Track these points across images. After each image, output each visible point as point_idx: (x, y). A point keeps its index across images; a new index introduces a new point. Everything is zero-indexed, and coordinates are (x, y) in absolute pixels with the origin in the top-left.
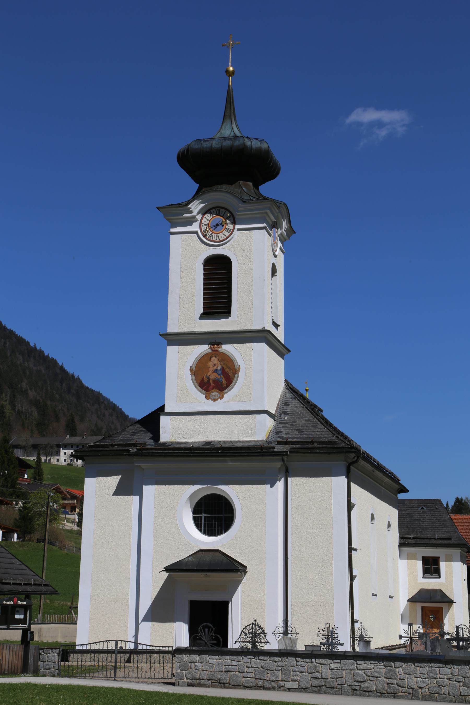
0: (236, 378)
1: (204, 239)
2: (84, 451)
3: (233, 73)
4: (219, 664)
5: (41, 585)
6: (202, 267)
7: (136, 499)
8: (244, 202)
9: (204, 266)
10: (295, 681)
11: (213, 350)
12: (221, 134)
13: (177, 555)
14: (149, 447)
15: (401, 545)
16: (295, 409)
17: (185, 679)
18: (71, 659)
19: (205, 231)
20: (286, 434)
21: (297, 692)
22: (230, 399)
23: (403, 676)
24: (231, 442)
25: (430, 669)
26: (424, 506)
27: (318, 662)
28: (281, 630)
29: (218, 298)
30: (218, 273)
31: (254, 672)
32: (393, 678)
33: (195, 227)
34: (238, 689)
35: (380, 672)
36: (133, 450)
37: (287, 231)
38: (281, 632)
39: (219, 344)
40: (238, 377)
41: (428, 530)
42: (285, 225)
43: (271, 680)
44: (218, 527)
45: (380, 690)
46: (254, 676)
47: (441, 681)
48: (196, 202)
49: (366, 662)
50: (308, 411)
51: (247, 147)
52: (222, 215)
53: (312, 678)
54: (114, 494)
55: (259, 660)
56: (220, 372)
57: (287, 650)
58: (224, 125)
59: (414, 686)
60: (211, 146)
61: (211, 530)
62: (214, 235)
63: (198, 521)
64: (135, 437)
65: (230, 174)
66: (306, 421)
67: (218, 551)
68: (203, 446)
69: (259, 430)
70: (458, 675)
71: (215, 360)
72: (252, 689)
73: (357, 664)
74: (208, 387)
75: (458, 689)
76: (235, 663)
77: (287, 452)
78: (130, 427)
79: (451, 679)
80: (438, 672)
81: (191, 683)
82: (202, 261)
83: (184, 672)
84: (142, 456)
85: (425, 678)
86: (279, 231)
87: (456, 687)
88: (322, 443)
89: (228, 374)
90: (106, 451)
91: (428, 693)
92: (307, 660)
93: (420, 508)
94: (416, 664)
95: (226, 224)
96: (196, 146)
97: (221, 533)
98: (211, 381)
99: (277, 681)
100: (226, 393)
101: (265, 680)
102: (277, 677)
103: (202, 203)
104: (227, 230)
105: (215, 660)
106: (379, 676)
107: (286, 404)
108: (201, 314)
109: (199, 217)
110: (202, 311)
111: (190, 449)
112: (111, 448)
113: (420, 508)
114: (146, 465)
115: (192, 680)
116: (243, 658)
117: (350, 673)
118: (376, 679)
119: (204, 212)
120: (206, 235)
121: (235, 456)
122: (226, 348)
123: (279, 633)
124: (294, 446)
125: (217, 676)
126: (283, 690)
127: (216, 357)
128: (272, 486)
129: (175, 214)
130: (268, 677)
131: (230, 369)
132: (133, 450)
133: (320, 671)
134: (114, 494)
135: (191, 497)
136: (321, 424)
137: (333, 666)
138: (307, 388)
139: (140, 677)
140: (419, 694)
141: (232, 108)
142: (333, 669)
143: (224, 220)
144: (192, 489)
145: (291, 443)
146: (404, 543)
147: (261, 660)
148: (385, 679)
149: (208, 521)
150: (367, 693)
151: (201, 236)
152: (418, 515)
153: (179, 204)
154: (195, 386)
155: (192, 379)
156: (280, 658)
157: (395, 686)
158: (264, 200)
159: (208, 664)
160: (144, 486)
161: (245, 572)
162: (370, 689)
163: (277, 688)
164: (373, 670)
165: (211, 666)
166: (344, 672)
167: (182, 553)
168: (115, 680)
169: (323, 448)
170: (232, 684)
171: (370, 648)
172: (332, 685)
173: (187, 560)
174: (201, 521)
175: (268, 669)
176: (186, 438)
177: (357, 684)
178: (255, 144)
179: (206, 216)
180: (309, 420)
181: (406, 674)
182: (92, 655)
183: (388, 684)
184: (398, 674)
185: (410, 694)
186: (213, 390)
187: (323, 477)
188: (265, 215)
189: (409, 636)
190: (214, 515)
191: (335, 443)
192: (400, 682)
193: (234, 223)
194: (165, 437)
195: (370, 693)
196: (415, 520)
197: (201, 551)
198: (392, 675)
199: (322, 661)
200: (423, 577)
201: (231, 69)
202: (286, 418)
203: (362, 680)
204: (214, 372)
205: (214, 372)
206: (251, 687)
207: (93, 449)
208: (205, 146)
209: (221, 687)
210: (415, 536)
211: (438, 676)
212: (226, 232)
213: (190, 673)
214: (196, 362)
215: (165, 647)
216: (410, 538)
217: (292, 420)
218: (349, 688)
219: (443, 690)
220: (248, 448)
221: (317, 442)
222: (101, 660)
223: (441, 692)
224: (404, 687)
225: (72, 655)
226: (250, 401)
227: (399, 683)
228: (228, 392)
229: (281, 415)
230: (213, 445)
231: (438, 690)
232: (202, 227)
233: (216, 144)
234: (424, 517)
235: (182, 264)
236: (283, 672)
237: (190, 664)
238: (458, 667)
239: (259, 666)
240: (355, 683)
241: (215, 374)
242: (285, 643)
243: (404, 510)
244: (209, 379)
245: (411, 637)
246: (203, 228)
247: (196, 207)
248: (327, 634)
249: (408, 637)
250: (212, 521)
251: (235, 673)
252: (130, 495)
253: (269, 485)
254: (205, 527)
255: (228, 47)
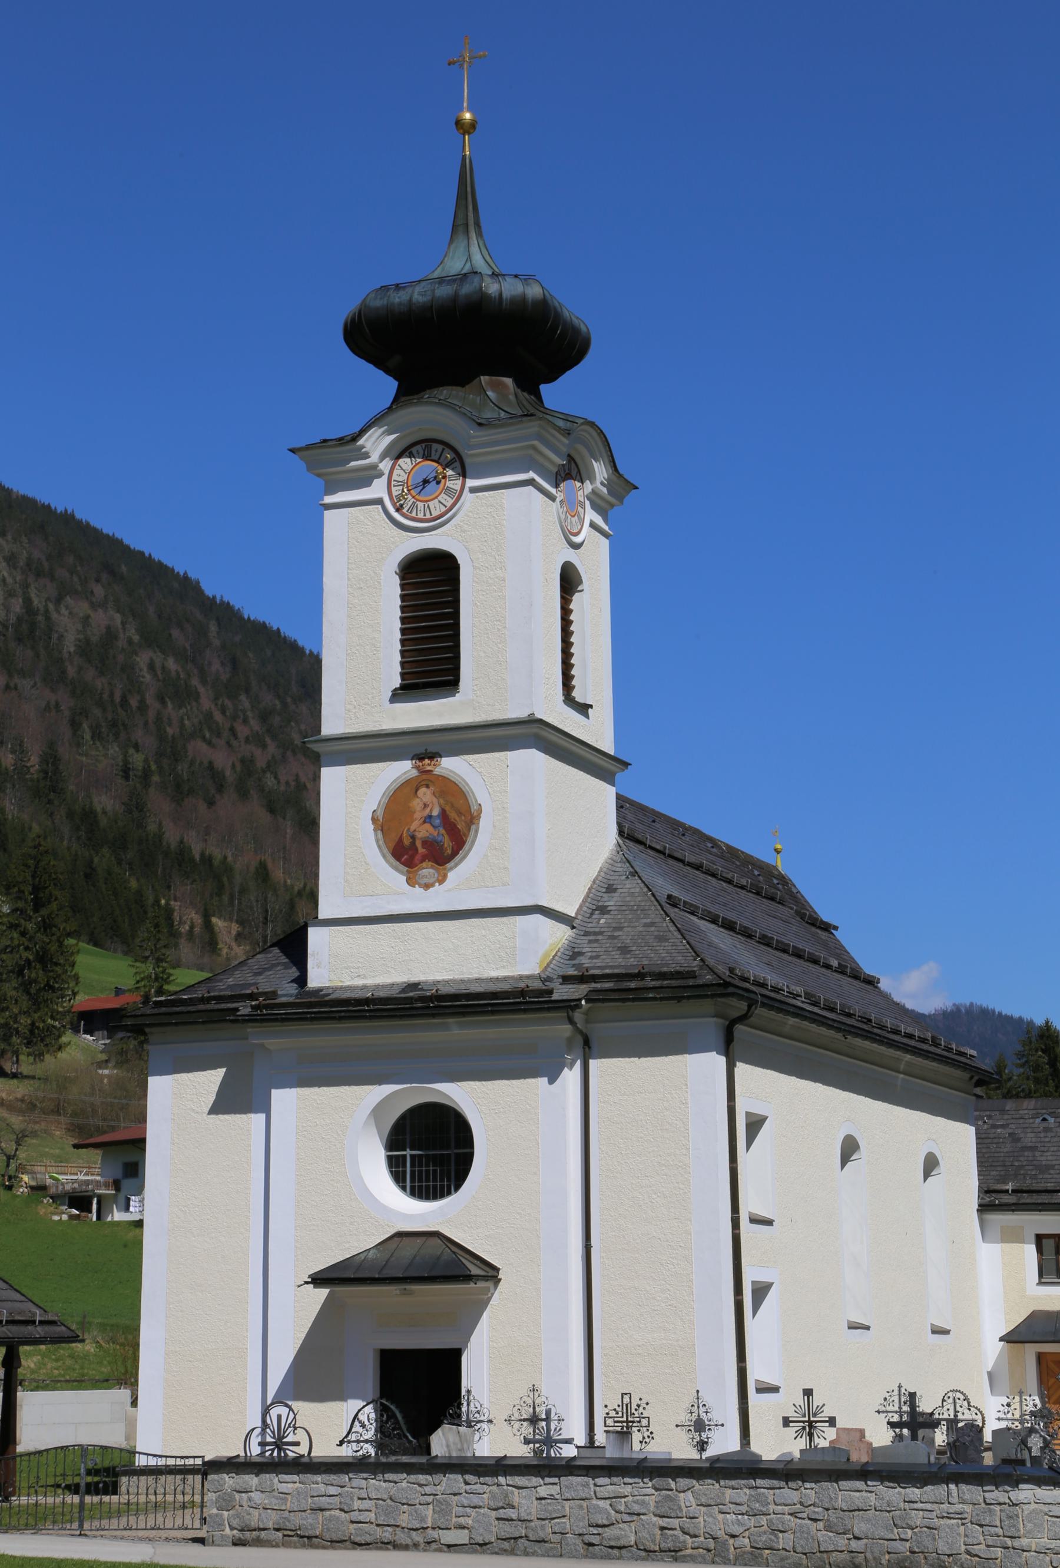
0: (472, 833)
1: (397, 516)
2: (142, 1015)
3: (473, 125)
4: (299, 1493)
5: (34, 1322)
6: (397, 581)
7: (257, 1120)
8: (480, 424)
9: (402, 578)
10: (462, 1527)
11: (423, 772)
12: (443, 270)
13: (347, 1246)
14: (284, 1000)
15: (984, 1208)
16: (628, 899)
17: (228, 1530)
18: (123, 1489)
19: (399, 497)
20: (591, 958)
21: (467, 1552)
22: (462, 884)
23: (694, 1510)
24: (462, 981)
25: (753, 1492)
26: (1049, 1114)
27: (511, 1483)
28: (523, 1412)
29: (431, 657)
30: (431, 587)
31: (374, 1509)
32: (672, 1515)
33: (378, 489)
34: (340, 1548)
35: (643, 1502)
36: (245, 1009)
37: (609, 485)
38: (525, 1416)
39: (433, 756)
40: (477, 832)
41: (1052, 1172)
42: (600, 471)
43: (410, 1526)
44: (442, 1180)
45: (643, 1544)
46: (373, 1520)
47: (778, 1519)
48: (374, 433)
49: (615, 1479)
50: (656, 903)
51: (489, 296)
52: (436, 458)
53: (498, 1519)
54: (210, 1113)
55: (385, 1481)
56: (437, 822)
57: (450, 1457)
58: (453, 246)
59: (719, 1533)
60: (410, 300)
61: (428, 1187)
62: (420, 505)
63: (397, 1166)
64: (260, 979)
65: (468, 358)
66: (646, 925)
67: (436, 1234)
68: (400, 993)
69: (525, 952)
70: (814, 1505)
71: (425, 794)
72: (370, 1549)
73: (595, 1485)
74: (412, 857)
75: (812, 1537)
76: (332, 1490)
77: (580, 1000)
78: (259, 956)
79: (799, 1515)
80: (771, 1498)
81: (240, 1539)
82: (395, 567)
83: (226, 1513)
84: (262, 1021)
85: (743, 1514)
86: (588, 487)
87: (808, 1533)
88: (662, 976)
89: (455, 825)
90: (189, 1012)
91: (748, 1549)
92: (488, 1480)
93: (1038, 1120)
94: (722, 1482)
95: (444, 477)
96: (378, 303)
97: (449, 1193)
98: (418, 844)
99: (423, 1528)
100: (451, 869)
101: (398, 1526)
102: (423, 1519)
103: (389, 432)
104: (448, 491)
105: (290, 1485)
106: (642, 1511)
107: (610, 889)
108: (396, 689)
109: (385, 466)
110: (397, 682)
111: (367, 1001)
112: (201, 1007)
113: (1038, 1120)
114: (278, 1042)
115: (242, 1530)
116: (350, 1479)
117: (581, 1507)
118: (635, 1518)
119: (404, 451)
120: (401, 506)
121: (464, 1014)
122: (451, 765)
123: (520, 1420)
124: (598, 986)
125: (297, 1520)
126: (436, 1550)
127: (427, 786)
128: (551, 1081)
129: (331, 459)
130: (404, 1520)
131: (460, 813)
132: (245, 1009)
133: (516, 1504)
134: (210, 1113)
135: (377, 1112)
136: (676, 933)
137: (543, 1491)
138: (779, 846)
139: (190, 1526)
140: (728, 1550)
141: (470, 208)
142: (545, 1499)
143: (440, 469)
144: (376, 1093)
145: (594, 978)
146: (991, 1202)
147: (390, 1481)
148: (655, 1519)
149: (420, 1165)
150: (616, 1552)
151: (391, 510)
152: (1032, 1135)
153: (341, 439)
154: (384, 856)
155: (377, 841)
156: (429, 1477)
157: (678, 1533)
158: (524, 419)
159: (276, 1494)
160: (273, 1091)
161: (497, 1281)
162: (621, 1543)
163: (422, 1546)
164: (630, 1498)
165: (281, 1499)
166: (567, 1504)
167: (358, 1240)
168: (80, 1535)
169: (661, 987)
170: (328, 1538)
171: (15, 1449)
172: (542, 1535)
173: (362, 1256)
174: (405, 1166)
175: (404, 1501)
176: (365, 977)
177: (595, 1532)
178: (511, 289)
179: (401, 461)
180: (652, 924)
181: (702, 1505)
182: (151, 1479)
183: (662, 1528)
184: (683, 1505)
185: (709, 1551)
186: (424, 864)
187: (666, 1055)
188: (531, 452)
189: (806, 1419)
190: (432, 1150)
191: (691, 975)
192: (687, 1524)
193: (464, 474)
194: (319, 977)
195: (624, 1551)
196: (1025, 1148)
197: (400, 1235)
198: (670, 1508)
199: (519, 1480)
200: (1040, 1283)
201: (468, 116)
202: (602, 921)
203: (606, 1522)
204: (425, 822)
205: (425, 822)
206: (368, 1544)
207: (163, 1010)
208: (397, 300)
209: (303, 1546)
210: (1018, 1185)
211: (772, 1507)
212: (446, 497)
213: (238, 1516)
214: (385, 800)
215: (187, 1457)
216: (1007, 1191)
217: (614, 925)
218: (578, 1541)
219: (781, 1540)
220: (494, 995)
221: (651, 974)
222: (143, 1490)
223: (776, 1546)
224: (696, 1536)
225: (124, 1480)
226: (504, 885)
227: (687, 1525)
228: (456, 865)
229: (592, 914)
230: (422, 989)
231: (771, 1540)
232: (394, 489)
233: (420, 294)
234: (1047, 1140)
235: (351, 576)
236: (437, 1509)
237: (237, 1496)
238: (813, 1485)
239: (385, 1497)
240: (591, 1529)
241: (427, 826)
242: (447, 1441)
243: (1003, 1126)
244: (413, 837)
245: (810, 1423)
246: (395, 491)
247: (376, 443)
248: (625, 1419)
249: (803, 1422)
250: (427, 1165)
251: (332, 1512)
252: (245, 1113)
253: (546, 1079)
254: (412, 1180)
255: (461, 66)
